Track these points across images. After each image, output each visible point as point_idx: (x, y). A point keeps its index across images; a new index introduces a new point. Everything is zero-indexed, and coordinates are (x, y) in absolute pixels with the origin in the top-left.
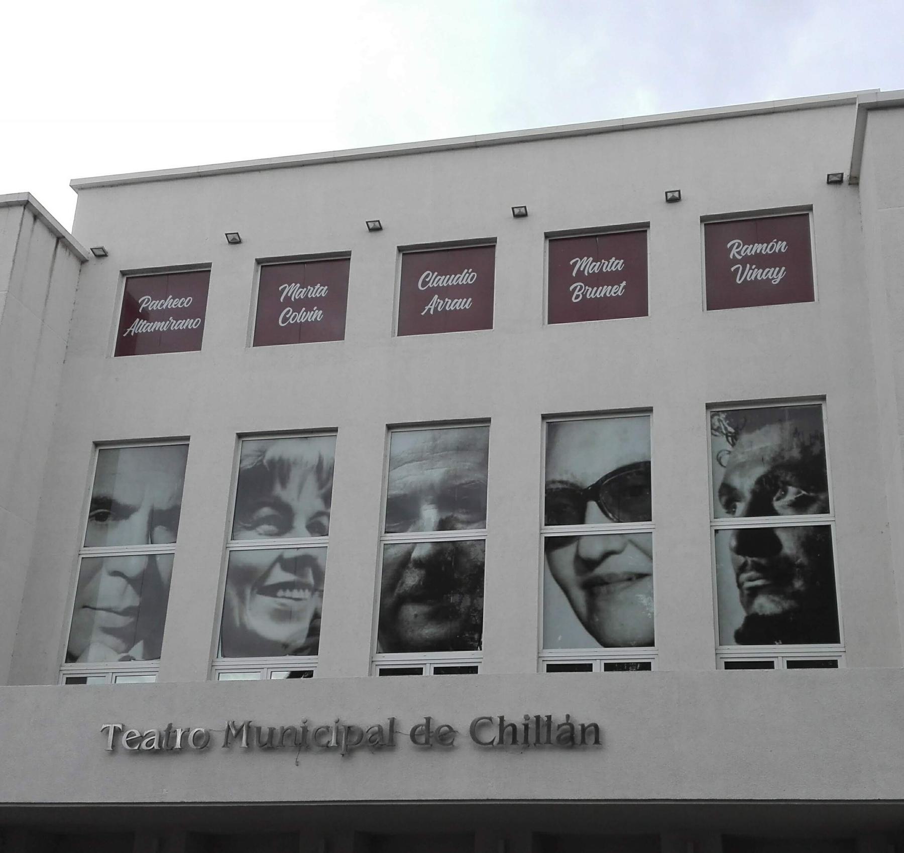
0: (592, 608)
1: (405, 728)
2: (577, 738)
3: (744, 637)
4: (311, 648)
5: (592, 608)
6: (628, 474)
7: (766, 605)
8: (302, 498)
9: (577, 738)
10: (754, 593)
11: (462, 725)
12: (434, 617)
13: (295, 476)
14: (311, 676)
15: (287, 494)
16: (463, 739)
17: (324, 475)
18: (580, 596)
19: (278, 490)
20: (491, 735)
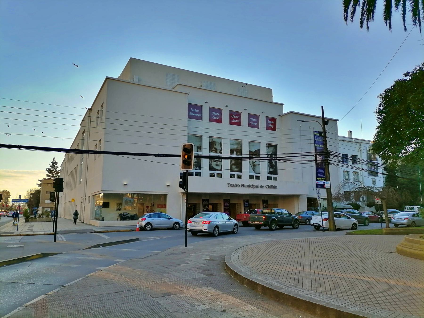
0: (254, 168)
1: (259, 186)
2: (275, 187)
3: (269, 173)
4: (221, 170)
5: (254, 168)
6: (134, 218)
7: (271, 170)
8: (218, 147)
9: (275, 187)
10: (270, 168)
11: (265, 186)
12: (236, 168)
13: (217, 144)
14: (351, 132)
15: (216, 147)
16: (265, 187)
17: (221, 144)
18: (253, 166)
19: (215, 146)
20: (267, 187)
